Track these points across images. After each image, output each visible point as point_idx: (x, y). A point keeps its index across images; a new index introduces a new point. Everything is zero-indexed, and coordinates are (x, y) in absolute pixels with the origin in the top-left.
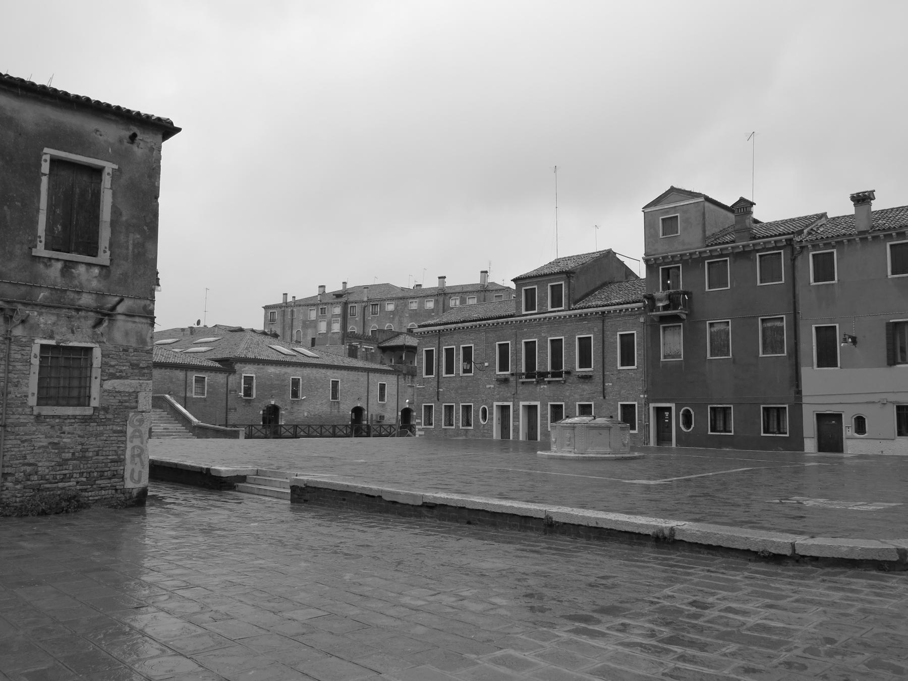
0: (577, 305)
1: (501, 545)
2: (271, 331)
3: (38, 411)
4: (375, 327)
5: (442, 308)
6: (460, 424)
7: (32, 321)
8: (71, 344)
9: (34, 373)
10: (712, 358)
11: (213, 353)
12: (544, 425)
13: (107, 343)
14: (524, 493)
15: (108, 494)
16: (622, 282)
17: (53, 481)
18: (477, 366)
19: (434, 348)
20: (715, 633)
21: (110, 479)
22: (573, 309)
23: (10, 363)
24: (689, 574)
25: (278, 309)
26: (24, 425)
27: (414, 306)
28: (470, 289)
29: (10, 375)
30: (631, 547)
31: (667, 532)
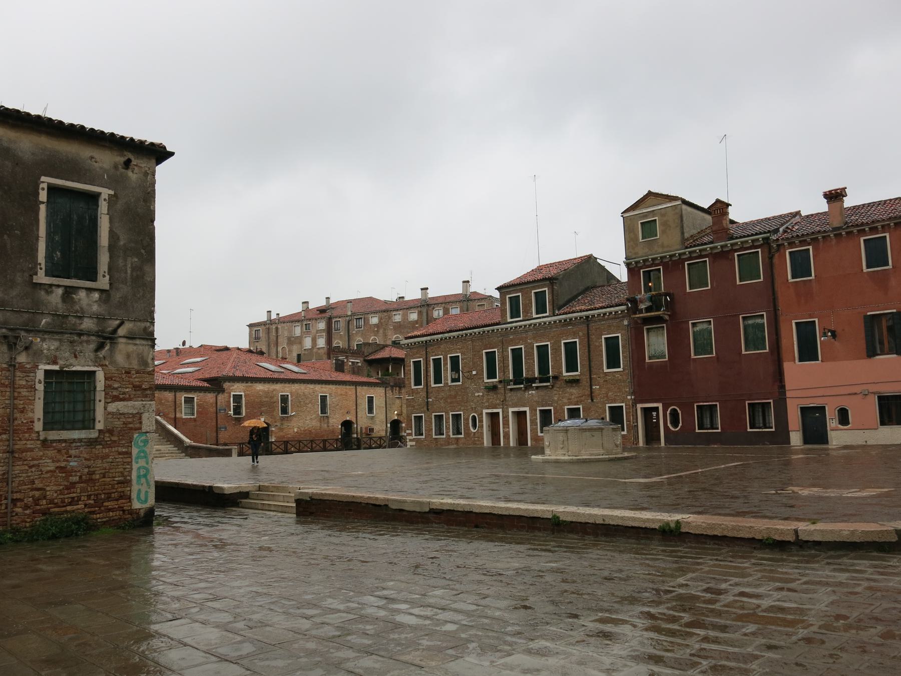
0: (561, 311)
1: (512, 546)
2: (257, 349)
3: (44, 436)
4: (361, 341)
5: (425, 319)
6: (451, 433)
7: (35, 348)
8: (74, 369)
9: (39, 399)
10: (696, 357)
11: (200, 373)
12: (534, 431)
13: (110, 366)
14: (527, 495)
15: (116, 516)
16: (604, 286)
17: (62, 504)
18: (466, 374)
19: (421, 359)
20: (733, 616)
21: (117, 500)
22: (557, 315)
23: (15, 390)
24: (699, 564)
25: (263, 326)
26: (31, 450)
27: (398, 318)
28: (452, 299)
29: (16, 402)
30: (638, 542)
31: (673, 525)
